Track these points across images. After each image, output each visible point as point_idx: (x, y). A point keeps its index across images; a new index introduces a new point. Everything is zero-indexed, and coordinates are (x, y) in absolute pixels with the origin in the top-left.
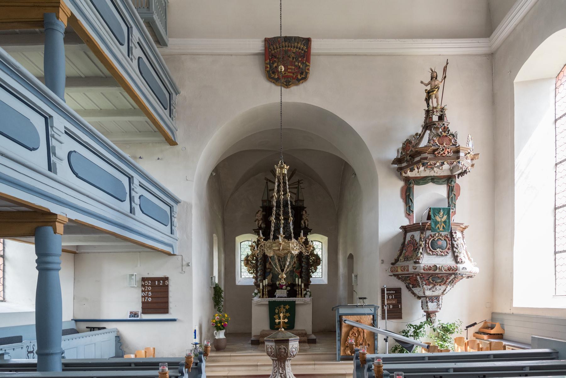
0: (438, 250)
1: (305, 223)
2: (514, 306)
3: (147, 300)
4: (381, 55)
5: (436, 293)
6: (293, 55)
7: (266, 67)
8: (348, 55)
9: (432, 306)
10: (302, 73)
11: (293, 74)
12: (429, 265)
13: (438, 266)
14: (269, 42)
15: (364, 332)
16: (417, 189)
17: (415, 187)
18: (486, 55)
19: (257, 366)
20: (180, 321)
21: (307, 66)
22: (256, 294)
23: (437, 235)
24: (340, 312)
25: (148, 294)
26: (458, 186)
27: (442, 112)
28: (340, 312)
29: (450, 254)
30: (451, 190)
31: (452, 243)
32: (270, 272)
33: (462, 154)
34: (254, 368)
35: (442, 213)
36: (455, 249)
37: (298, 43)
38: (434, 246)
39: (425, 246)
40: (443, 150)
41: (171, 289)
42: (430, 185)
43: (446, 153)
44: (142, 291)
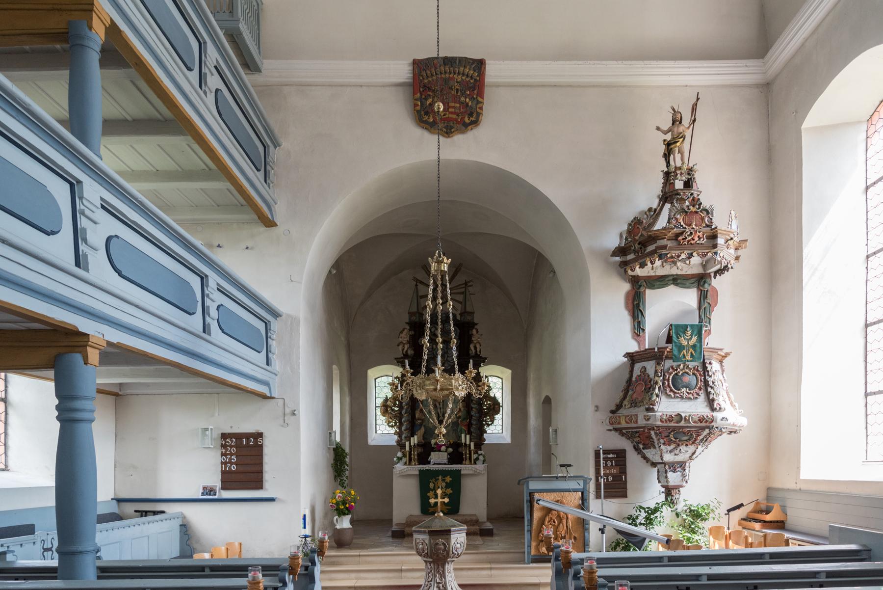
0: (684, 390)
1: (475, 348)
2: (802, 477)
3: (230, 468)
4: (594, 86)
5: (680, 458)
6: (457, 86)
7: (415, 105)
8: (543, 86)
9: (673, 478)
10: (471, 115)
11: (458, 115)
12: (669, 414)
13: (683, 415)
14: (420, 66)
15: (567, 518)
16: (650, 295)
17: (648, 292)
18: (758, 86)
19: (401, 571)
20: (281, 501)
21: (478, 102)
23: (682, 366)
24: (531, 487)
25: (230, 459)
27: (689, 174)
28: (531, 487)
29: (703, 396)
30: (703, 297)
31: (705, 379)
32: (421, 425)
33: (720, 241)
34: (396, 574)
35: (689, 333)
36: (709, 389)
37: (465, 67)
39: (664, 384)
40: (691, 233)
41: (266, 451)
42: (672, 289)
43: (696, 239)
44: (222, 454)
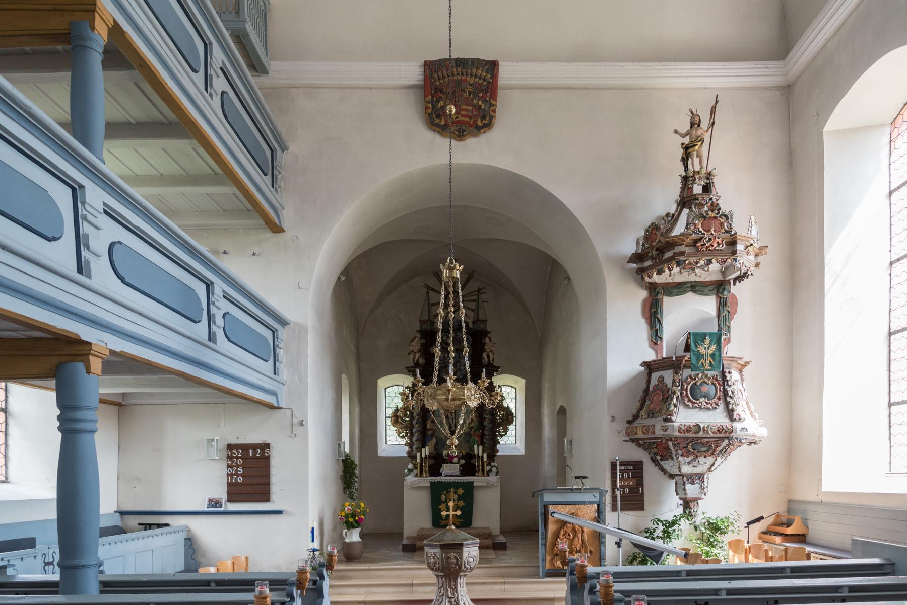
0: (702, 400)
1: (488, 357)
2: (824, 489)
3: (236, 479)
4: (610, 88)
5: (698, 470)
6: (470, 88)
7: (427, 108)
8: (558, 88)
9: (692, 490)
10: (484, 118)
11: (470, 118)
12: (687, 425)
13: (702, 426)
14: (431, 68)
15: (583, 531)
16: (668, 302)
17: (666, 299)
19: (412, 585)
20: (288, 513)
21: (491, 105)
22: (410, 471)
23: (700, 376)
24: (545, 500)
25: (237, 471)
26: (735, 298)
27: (708, 179)
28: (545, 500)
29: (722, 406)
30: (722, 304)
31: (724, 388)
32: (432, 436)
34: (407, 589)
35: (708, 341)
36: (729, 399)
37: (477, 69)
38: (695, 393)
39: (682, 393)
40: (710, 239)
41: (274, 462)
42: (690, 297)
43: (715, 245)
44: (228, 466)
